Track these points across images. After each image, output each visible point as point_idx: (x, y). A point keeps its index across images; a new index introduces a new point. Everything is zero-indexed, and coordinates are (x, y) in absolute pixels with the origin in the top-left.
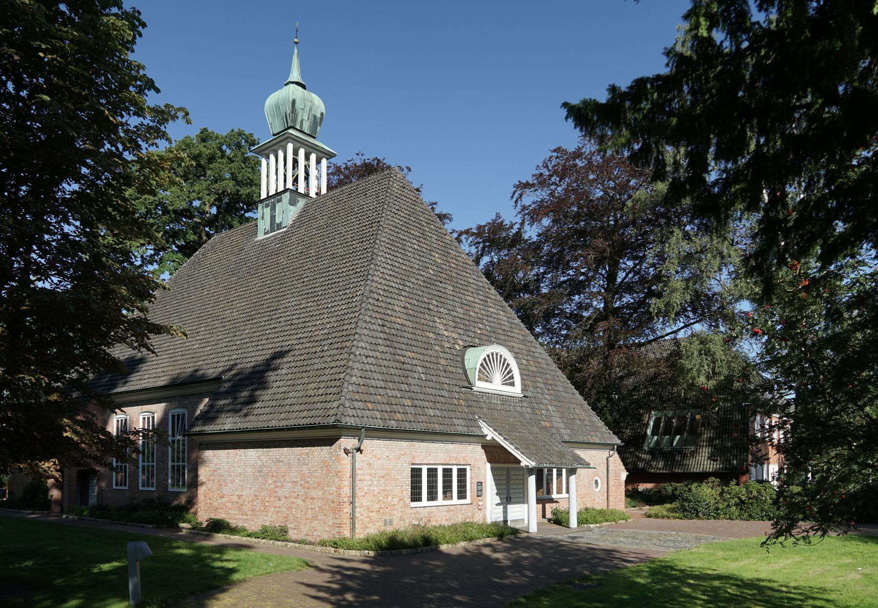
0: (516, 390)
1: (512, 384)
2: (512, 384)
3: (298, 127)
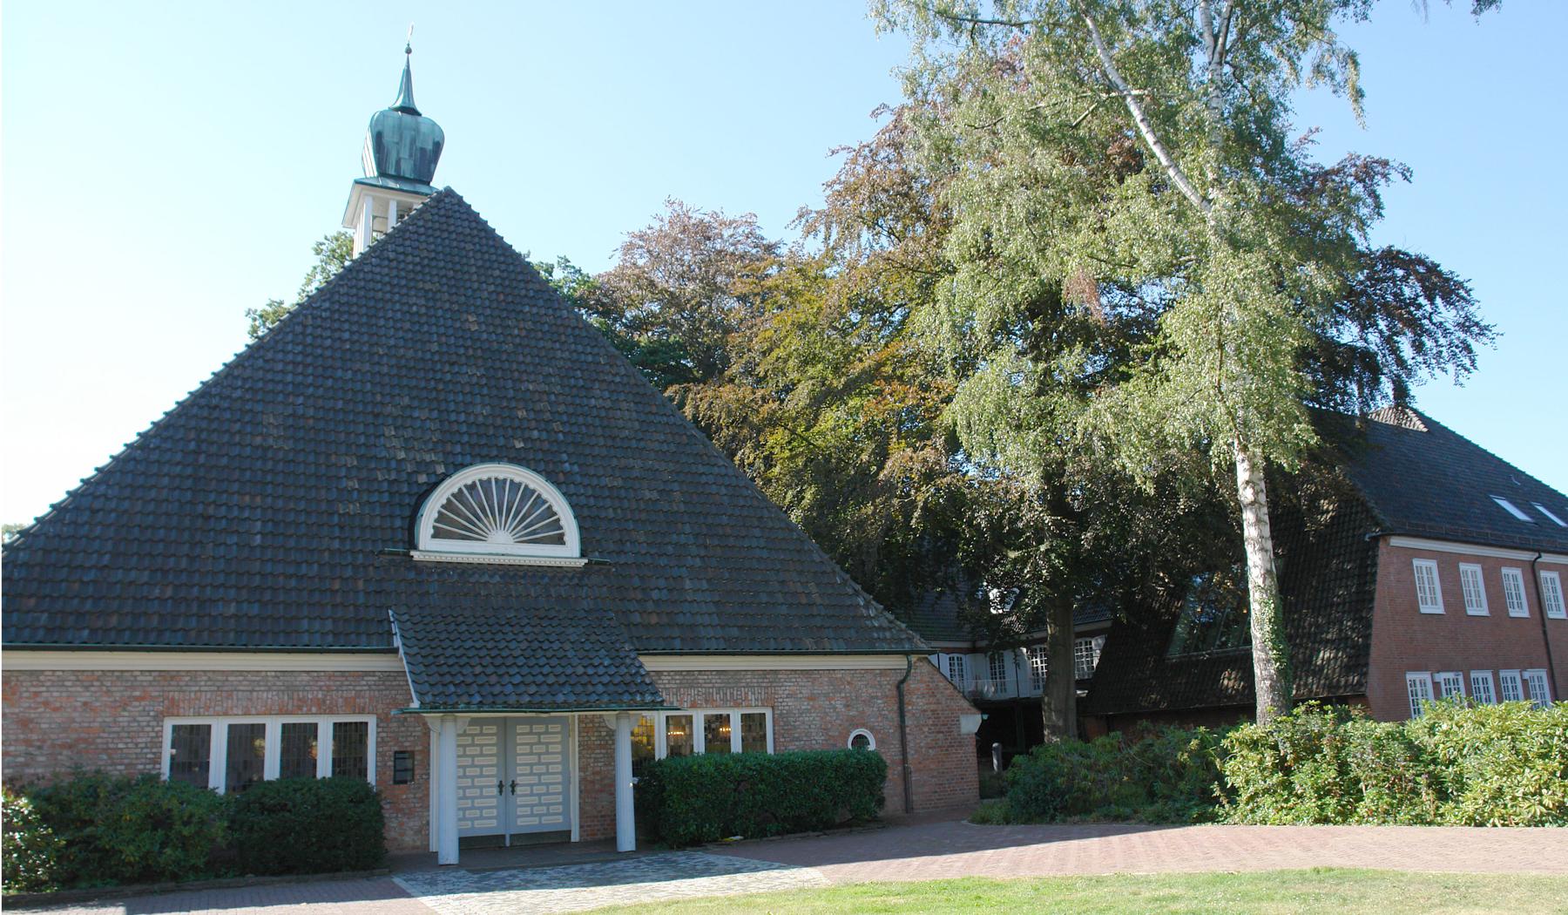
0: (569, 553)
1: (559, 540)
2: (559, 540)
3: (392, 172)
